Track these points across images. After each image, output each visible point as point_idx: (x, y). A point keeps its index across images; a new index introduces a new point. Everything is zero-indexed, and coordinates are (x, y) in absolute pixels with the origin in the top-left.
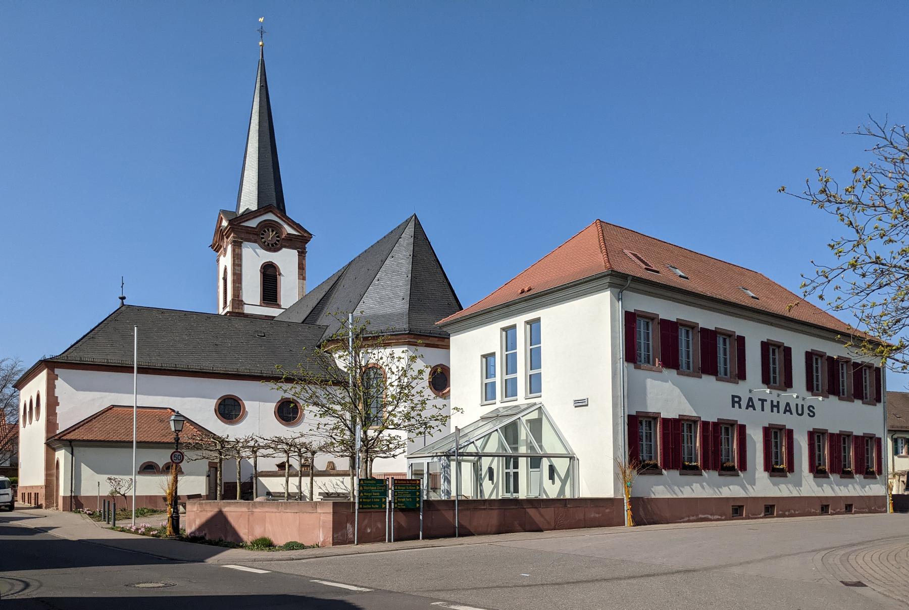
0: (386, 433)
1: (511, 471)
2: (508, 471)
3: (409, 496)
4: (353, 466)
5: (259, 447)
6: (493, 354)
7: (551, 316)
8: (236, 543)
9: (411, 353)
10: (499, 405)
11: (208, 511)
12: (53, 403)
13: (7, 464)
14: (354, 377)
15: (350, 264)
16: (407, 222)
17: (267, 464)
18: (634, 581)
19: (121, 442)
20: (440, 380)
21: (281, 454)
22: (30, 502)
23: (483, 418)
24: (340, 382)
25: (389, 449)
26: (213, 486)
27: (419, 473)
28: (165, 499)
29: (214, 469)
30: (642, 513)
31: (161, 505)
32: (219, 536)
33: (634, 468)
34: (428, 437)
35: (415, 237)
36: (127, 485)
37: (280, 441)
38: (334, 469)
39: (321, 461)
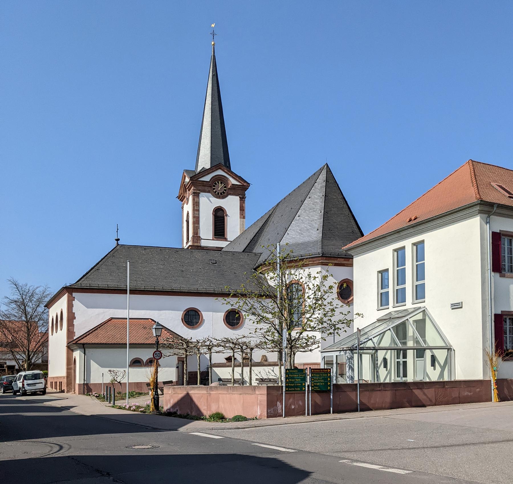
0: (305, 334)
1: (401, 360)
2: (398, 360)
3: (323, 381)
4: (280, 359)
5: (213, 346)
6: (387, 270)
7: (433, 239)
8: (199, 416)
9: (324, 273)
10: (391, 309)
11: (179, 393)
12: (71, 317)
13: (40, 361)
14: (281, 293)
15: (278, 205)
16: (321, 170)
17: (219, 358)
18: (496, 445)
19: (117, 344)
20: (346, 291)
21: (229, 351)
22: (56, 388)
23: (379, 320)
24: (269, 294)
25: (307, 345)
26: (181, 374)
27: (329, 363)
28: (148, 385)
29: (182, 362)
30: (506, 391)
31: (145, 389)
32: (187, 411)
33: (500, 356)
34: (337, 336)
35: (327, 181)
36: (122, 375)
37: (228, 341)
38: (266, 361)
39: (257, 355)
